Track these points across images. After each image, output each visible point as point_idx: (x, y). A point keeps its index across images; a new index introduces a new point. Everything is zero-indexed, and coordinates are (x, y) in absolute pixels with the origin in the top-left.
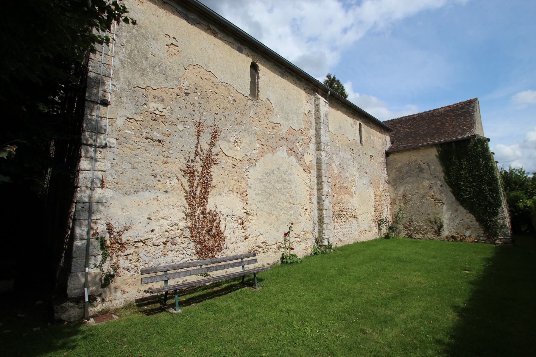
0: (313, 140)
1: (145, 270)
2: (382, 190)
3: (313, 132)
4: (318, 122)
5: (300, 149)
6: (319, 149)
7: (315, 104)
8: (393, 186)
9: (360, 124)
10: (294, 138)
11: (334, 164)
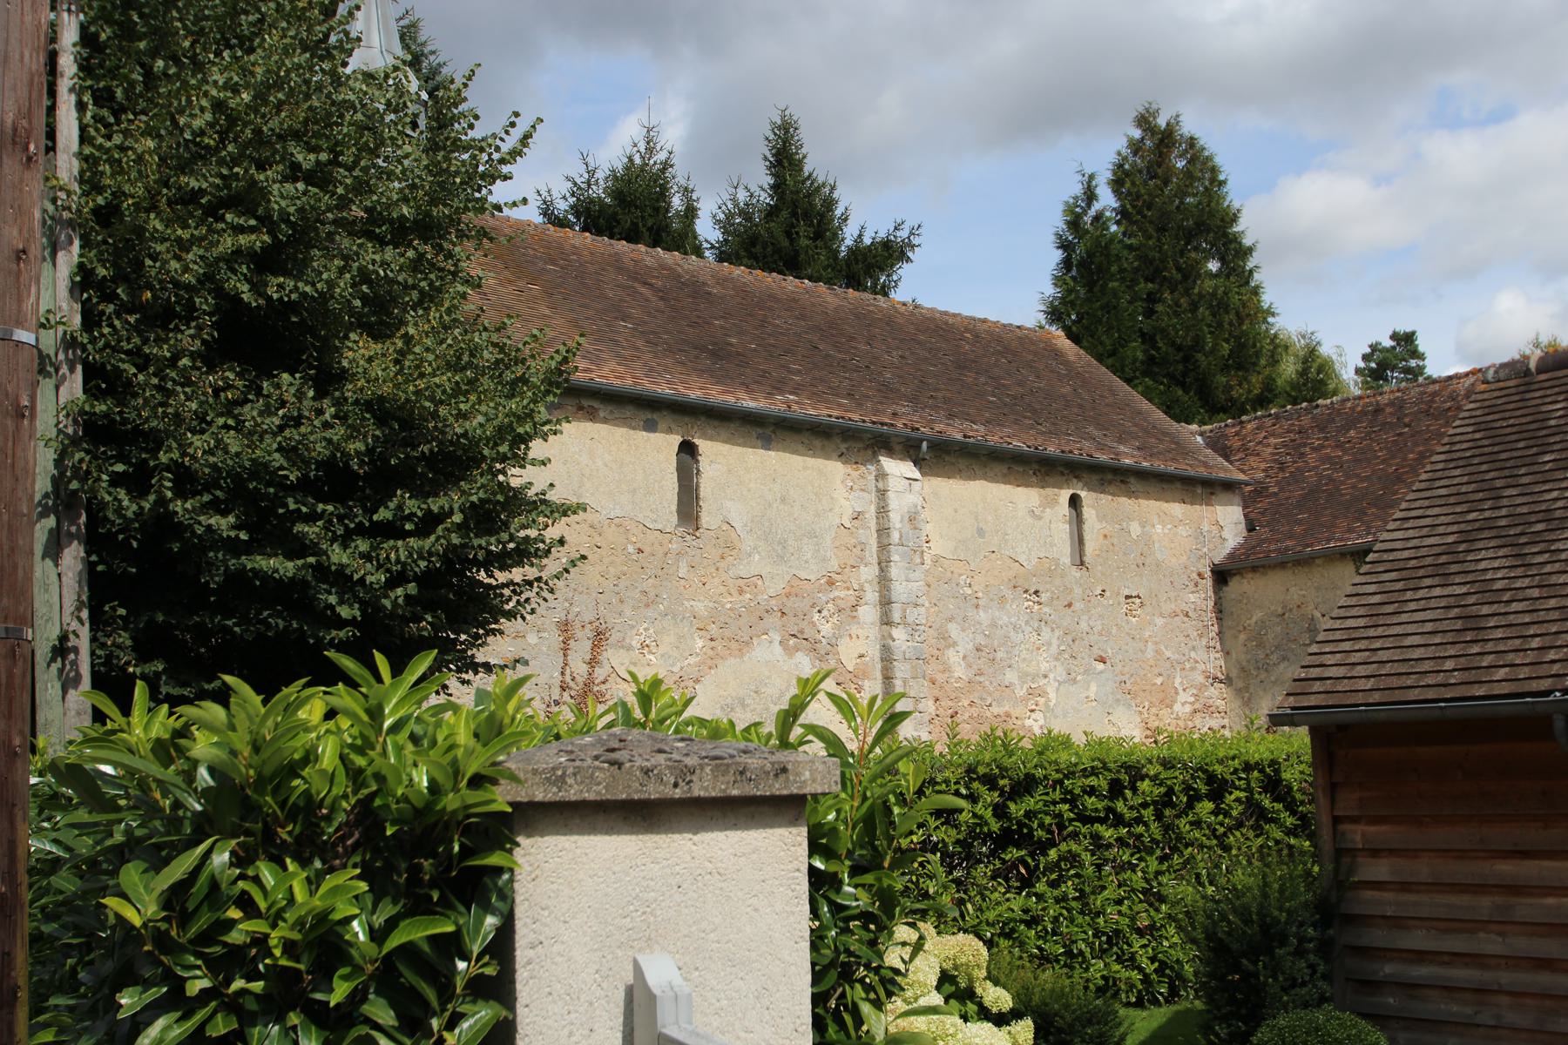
0: (872, 595)
1: (948, 453)
2: (1188, 708)
3: (869, 572)
4: (886, 542)
5: (826, 629)
6: (886, 621)
7: (878, 490)
8: (1239, 691)
9: (1074, 501)
10: (807, 602)
11: (951, 653)
